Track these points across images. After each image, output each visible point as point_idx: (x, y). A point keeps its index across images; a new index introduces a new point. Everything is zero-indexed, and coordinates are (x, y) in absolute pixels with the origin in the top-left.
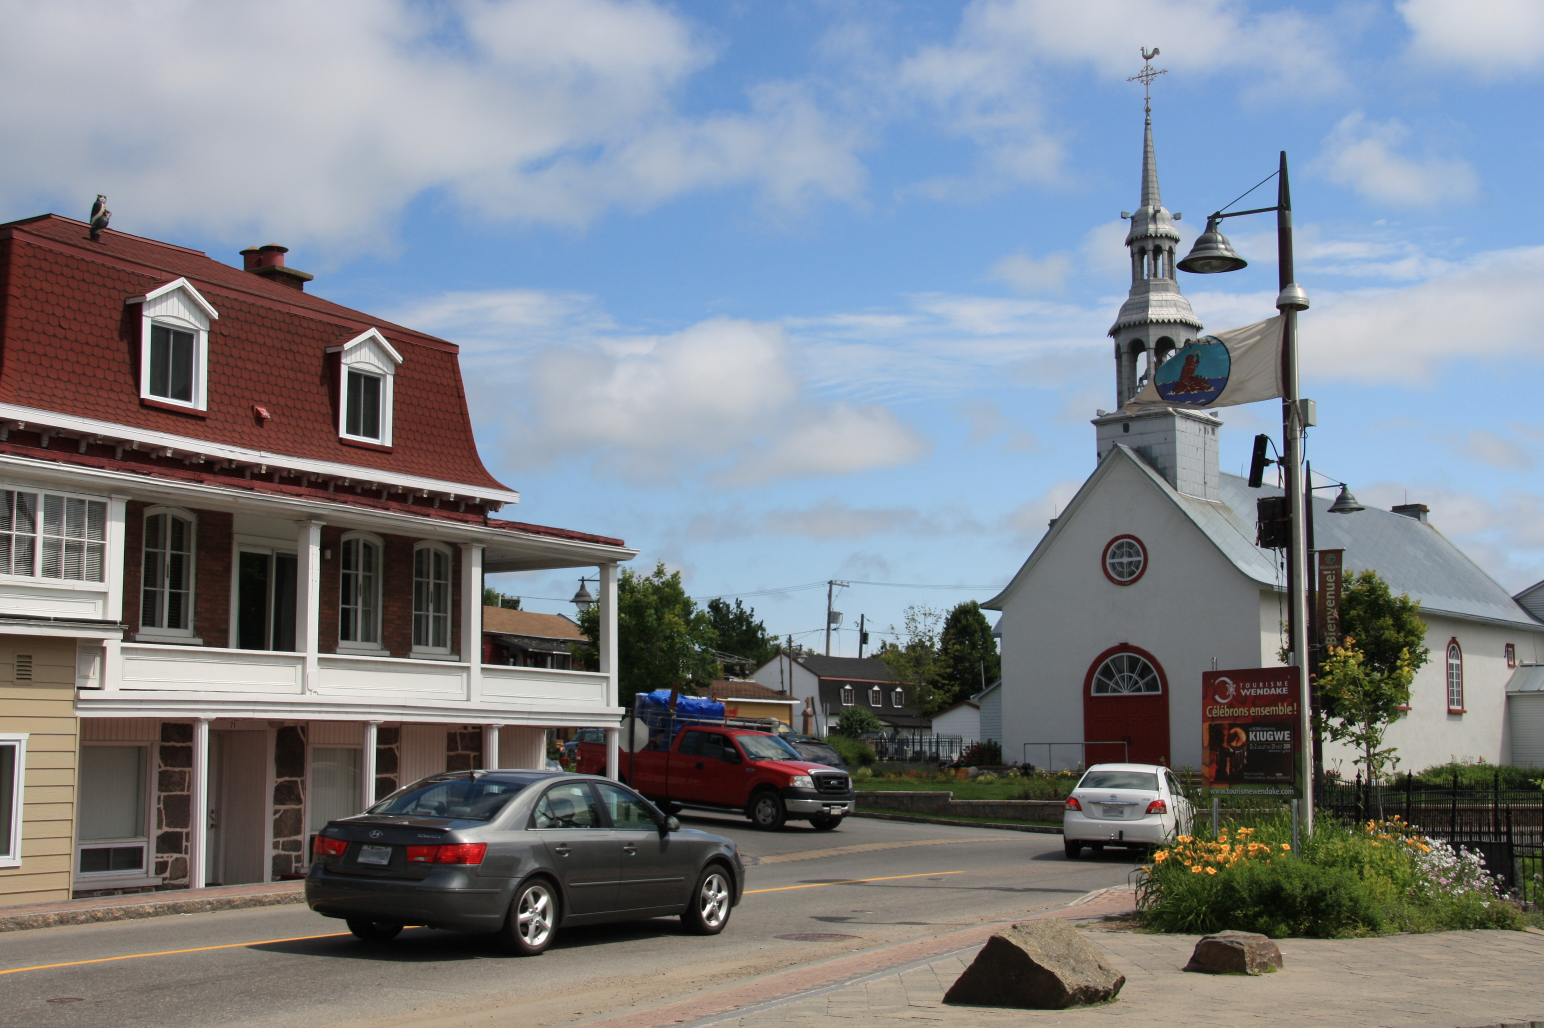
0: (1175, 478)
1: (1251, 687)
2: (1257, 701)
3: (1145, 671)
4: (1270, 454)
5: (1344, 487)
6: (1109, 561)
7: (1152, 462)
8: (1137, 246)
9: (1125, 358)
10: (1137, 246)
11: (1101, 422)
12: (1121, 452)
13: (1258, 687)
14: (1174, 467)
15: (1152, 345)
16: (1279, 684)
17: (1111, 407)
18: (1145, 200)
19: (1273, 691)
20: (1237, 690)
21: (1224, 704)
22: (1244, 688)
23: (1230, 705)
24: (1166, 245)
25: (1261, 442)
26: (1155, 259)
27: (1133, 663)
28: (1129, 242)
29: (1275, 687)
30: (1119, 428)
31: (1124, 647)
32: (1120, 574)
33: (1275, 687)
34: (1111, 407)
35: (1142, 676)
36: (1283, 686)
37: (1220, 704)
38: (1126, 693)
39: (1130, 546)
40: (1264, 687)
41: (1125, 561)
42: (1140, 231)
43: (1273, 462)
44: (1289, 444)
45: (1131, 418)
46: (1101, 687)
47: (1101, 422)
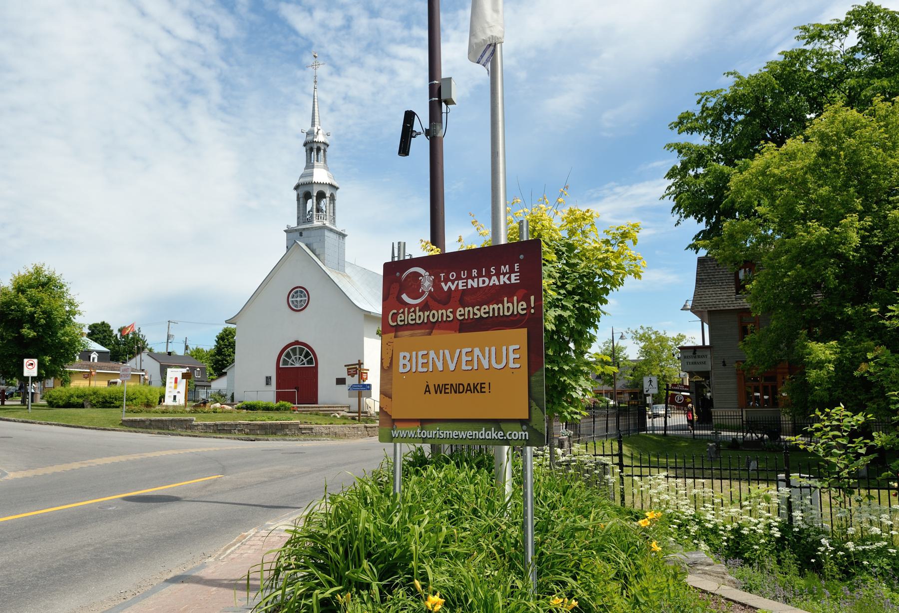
0: (322, 258)
1: (459, 278)
2: (467, 298)
3: (307, 355)
4: (417, 127)
6: (290, 299)
8: (309, 146)
9: (301, 200)
10: (309, 146)
11: (289, 231)
13: (470, 277)
14: (324, 253)
16: (505, 269)
17: (294, 224)
18: (313, 124)
19: (494, 280)
20: (436, 284)
22: (446, 280)
23: (424, 307)
25: (409, 117)
26: (317, 154)
27: (302, 350)
28: (305, 145)
29: (498, 275)
30: (298, 234)
31: (297, 343)
32: (296, 306)
33: (498, 275)
34: (294, 224)
36: (512, 271)
37: (409, 306)
38: (297, 365)
39: (301, 292)
40: (480, 275)
41: (298, 298)
42: (310, 138)
43: (420, 134)
44: (435, 115)
46: (285, 362)
47: (289, 231)
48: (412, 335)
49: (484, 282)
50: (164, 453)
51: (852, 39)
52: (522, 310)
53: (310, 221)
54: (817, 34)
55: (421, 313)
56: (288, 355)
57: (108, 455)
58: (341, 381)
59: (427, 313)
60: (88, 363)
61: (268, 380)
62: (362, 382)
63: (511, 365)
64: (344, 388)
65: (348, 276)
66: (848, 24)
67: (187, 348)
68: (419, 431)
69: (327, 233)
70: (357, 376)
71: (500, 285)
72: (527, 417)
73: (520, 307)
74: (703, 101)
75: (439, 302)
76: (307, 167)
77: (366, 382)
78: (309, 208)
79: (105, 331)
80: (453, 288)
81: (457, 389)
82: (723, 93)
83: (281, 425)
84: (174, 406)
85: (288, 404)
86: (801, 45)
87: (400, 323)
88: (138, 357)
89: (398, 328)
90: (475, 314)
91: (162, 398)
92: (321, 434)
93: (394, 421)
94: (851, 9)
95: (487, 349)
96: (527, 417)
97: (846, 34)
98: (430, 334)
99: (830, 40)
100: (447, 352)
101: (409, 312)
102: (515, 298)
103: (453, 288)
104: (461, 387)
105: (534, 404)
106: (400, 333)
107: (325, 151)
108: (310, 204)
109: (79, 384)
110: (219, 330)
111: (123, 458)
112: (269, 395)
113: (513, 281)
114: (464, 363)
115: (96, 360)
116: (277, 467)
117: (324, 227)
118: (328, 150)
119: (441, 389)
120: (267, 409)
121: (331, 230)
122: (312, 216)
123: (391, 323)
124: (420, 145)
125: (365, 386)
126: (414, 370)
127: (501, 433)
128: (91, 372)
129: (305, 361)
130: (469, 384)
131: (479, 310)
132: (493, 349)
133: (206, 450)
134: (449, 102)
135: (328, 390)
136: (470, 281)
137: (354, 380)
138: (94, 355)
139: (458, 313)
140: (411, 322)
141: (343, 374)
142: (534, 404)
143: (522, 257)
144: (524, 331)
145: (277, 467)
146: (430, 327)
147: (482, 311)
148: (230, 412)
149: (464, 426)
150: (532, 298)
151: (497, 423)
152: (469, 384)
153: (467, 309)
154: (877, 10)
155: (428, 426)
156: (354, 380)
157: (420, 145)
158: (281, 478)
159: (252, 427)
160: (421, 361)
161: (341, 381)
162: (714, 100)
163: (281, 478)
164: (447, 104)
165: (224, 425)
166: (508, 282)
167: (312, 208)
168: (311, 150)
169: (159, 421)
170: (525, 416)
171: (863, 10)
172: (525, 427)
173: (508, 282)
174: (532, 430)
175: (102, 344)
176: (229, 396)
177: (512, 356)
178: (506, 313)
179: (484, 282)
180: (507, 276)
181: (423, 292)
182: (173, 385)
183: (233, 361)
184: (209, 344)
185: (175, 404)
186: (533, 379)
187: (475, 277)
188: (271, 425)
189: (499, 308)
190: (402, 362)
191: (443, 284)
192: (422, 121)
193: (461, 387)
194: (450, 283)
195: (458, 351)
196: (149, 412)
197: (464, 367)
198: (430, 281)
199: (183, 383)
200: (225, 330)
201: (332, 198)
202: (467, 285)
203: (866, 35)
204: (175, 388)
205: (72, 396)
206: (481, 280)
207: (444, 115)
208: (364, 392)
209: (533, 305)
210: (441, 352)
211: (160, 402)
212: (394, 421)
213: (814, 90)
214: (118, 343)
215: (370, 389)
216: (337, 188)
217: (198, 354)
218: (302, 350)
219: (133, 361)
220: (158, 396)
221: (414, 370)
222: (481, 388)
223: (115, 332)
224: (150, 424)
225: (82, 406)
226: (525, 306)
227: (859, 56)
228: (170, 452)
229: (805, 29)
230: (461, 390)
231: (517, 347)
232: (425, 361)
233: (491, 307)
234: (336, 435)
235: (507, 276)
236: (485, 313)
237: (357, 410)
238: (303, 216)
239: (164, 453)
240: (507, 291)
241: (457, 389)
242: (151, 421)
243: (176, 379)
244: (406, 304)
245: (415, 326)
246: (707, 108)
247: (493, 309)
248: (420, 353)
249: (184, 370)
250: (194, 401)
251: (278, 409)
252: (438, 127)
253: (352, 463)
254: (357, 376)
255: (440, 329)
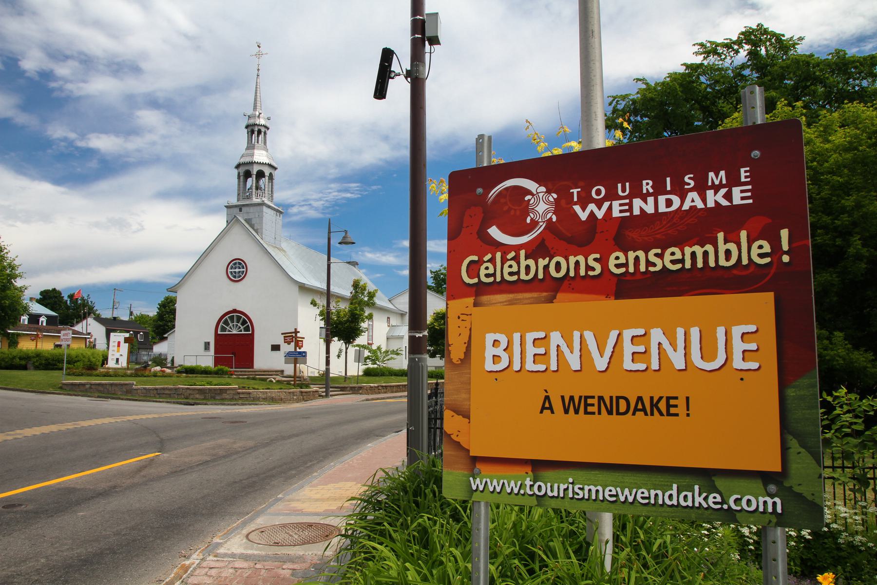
1: (612, 196)
3: (244, 323)
4: (395, 67)
5: (346, 232)
6: (229, 270)
7: (252, 226)
9: (242, 178)
12: (238, 220)
14: (262, 228)
15: (255, 173)
17: (234, 201)
18: (255, 108)
19: (693, 200)
20: (563, 207)
21: (517, 248)
22: (584, 202)
23: (536, 250)
24: (263, 129)
27: (239, 318)
28: (247, 127)
29: (701, 188)
31: (235, 311)
32: (235, 277)
33: (701, 188)
35: (243, 324)
36: (733, 181)
37: (505, 249)
38: (235, 332)
39: (240, 264)
40: (659, 190)
42: (252, 121)
44: (417, 56)
45: (244, 205)
46: (223, 329)
48: (511, 303)
49: (669, 203)
50: (99, 421)
51: (743, 55)
52: (761, 256)
53: (249, 197)
54: (710, 50)
55: (531, 262)
56: (226, 323)
57: (40, 424)
58: (275, 348)
59: (542, 262)
60: (36, 326)
61: (207, 346)
62: (298, 350)
63: (738, 363)
64: (280, 356)
65: (284, 251)
66: (739, 42)
67: (131, 314)
68: (528, 482)
69: (265, 209)
70: (293, 344)
71: (707, 210)
72: (779, 469)
73: (755, 251)
74: (614, 103)
75: (570, 241)
76: (247, 148)
77: (302, 350)
78: (248, 186)
79: (56, 297)
80: (600, 214)
81: (612, 406)
82: (631, 97)
83: (220, 389)
84: (115, 369)
85: (226, 369)
86: (699, 60)
87: (484, 279)
88: (84, 322)
89: (480, 290)
90: (649, 263)
91: (105, 359)
92: (258, 399)
93: (475, 460)
94: (744, 30)
95: (680, 332)
96: (779, 469)
97: (737, 52)
98: (551, 300)
99: (723, 57)
100: (589, 336)
101: (504, 260)
102: (743, 234)
103: (600, 214)
104: (622, 403)
105: (793, 443)
106: (485, 298)
107: (265, 133)
108: (251, 182)
109: (26, 345)
110: (161, 299)
111: (54, 428)
112: (207, 361)
113: (737, 200)
114: (627, 357)
115: (45, 324)
116: (220, 441)
117: (262, 204)
118: (268, 132)
119: (575, 405)
120: (205, 372)
121: (269, 207)
122: (251, 194)
123: (467, 280)
124: (399, 88)
125: (300, 353)
126: (516, 366)
127: (714, 499)
128: (37, 335)
129: (242, 328)
130: (640, 399)
131: (660, 256)
132: (695, 332)
133: (144, 417)
134: (434, 41)
135: (264, 359)
136: (637, 203)
137: (291, 347)
138: (43, 319)
139: (612, 262)
140: (508, 278)
141: (280, 341)
142: (793, 443)
143: (756, 154)
144: (770, 296)
145: (220, 441)
146: (551, 288)
147: (668, 257)
148: (170, 376)
149: (629, 478)
150: (784, 234)
151: (707, 477)
152: (640, 399)
153: (631, 255)
154: (766, 32)
155: (549, 474)
156: (291, 347)
157: (399, 88)
158: (224, 457)
159: (191, 392)
160: (531, 350)
161: (275, 348)
162: (624, 103)
163: (224, 457)
164: (431, 44)
165: (164, 389)
166: (724, 203)
167: (252, 186)
168: (253, 132)
169: (99, 384)
170: (775, 466)
171: (753, 30)
172: (772, 488)
173: (724, 203)
174: (789, 495)
175: (52, 309)
176: (169, 360)
177: (738, 346)
178: (722, 262)
179: (669, 203)
180: (723, 191)
181: (534, 224)
182: (116, 348)
183: (174, 326)
184: (152, 312)
185: (117, 366)
186: (791, 392)
187: (649, 194)
188: (210, 390)
189: (706, 254)
190: (490, 351)
191: (577, 208)
192: (402, 62)
193: (622, 403)
194: (592, 207)
195: (614, 334)
196: (90, 375)
197: (628, 365)
198: (548, 202)
199: (125, 347)
200: (167, 298)
201: (271, 177)
202: (631, 210)
203: (753, 54)
204: (118, 351)
205: (14, 357)
206: (662, 199)
207: (427, 56)
208: (300, 359)
209: (785, 247)
210: (576, 335)
211: (103, 364)
212: (475, 460)
213: (708, 99)
214: (68, 308)
215: (305, 356)
216: (275, 169)
217: (142, 319)
218: (239, 318)
219: (80, 325)
220: (101, 359)
221: (516, 366)
222: (669, 406)
223: (66, 298)
224: (90, 388)
225: (25, 368)
226: (767, 248)
227: (747, 72)
228: (106, 421)
229: (702, 45)
230: (623, 408)
231: (752, 328)
232: (542, 351)
233: (688, 250)
234: (273, 400)
235: (723, 191)
236: (673, 262)
237: (292, 374)
238: (244, 192)
239: (99, 421)
240: (727, 220)
241: (612, 406)
242: (91, 384)
243: (119, 343)
244: (498, 245)
245: (518, 286)
246: (618, 110)
247: (693, 254)
248: (530, 337)
249: (127, 335)
250: (137, 363)
251: (216, 373)
252: (421, 68)
253: (297, 435)
254: (293, 344)
255: (573, 290)
